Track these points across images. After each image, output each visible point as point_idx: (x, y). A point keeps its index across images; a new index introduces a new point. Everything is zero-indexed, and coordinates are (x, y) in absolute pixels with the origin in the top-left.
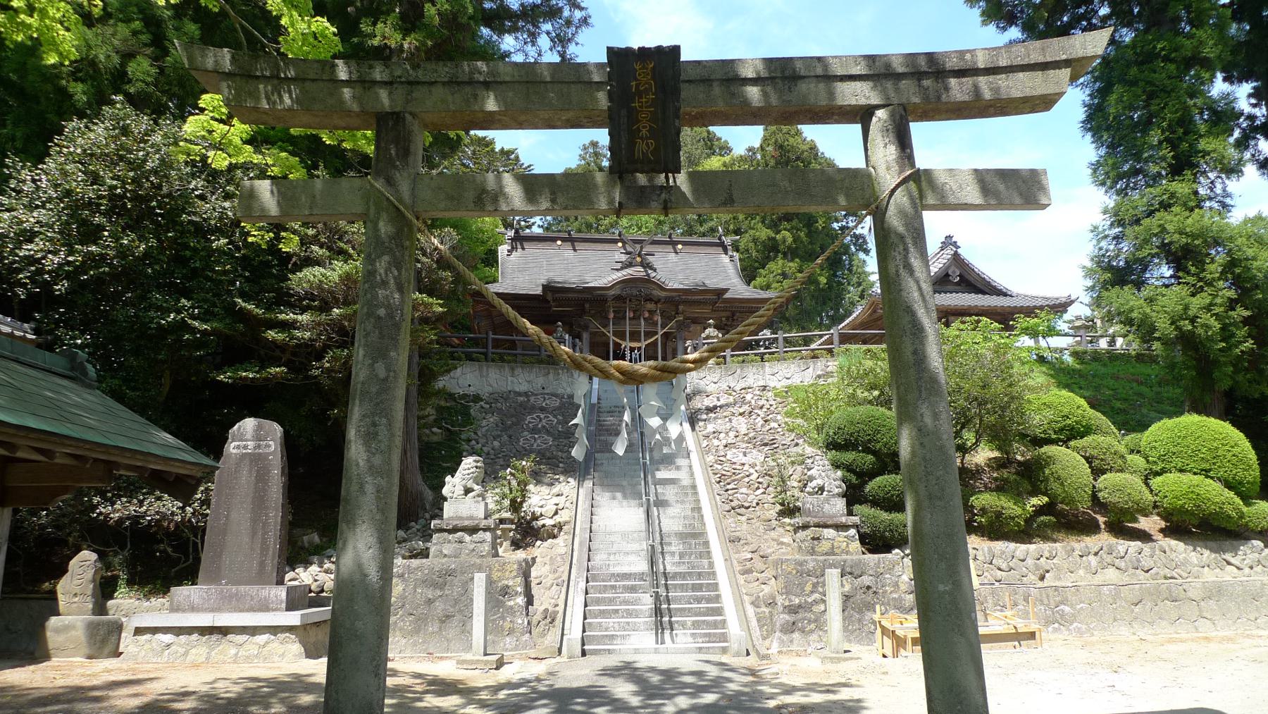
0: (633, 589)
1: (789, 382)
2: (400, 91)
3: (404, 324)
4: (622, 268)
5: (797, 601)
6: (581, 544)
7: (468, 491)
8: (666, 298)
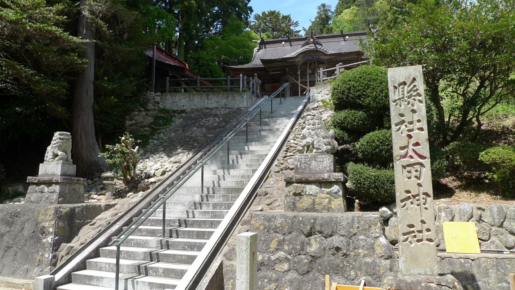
8: (328, 60)
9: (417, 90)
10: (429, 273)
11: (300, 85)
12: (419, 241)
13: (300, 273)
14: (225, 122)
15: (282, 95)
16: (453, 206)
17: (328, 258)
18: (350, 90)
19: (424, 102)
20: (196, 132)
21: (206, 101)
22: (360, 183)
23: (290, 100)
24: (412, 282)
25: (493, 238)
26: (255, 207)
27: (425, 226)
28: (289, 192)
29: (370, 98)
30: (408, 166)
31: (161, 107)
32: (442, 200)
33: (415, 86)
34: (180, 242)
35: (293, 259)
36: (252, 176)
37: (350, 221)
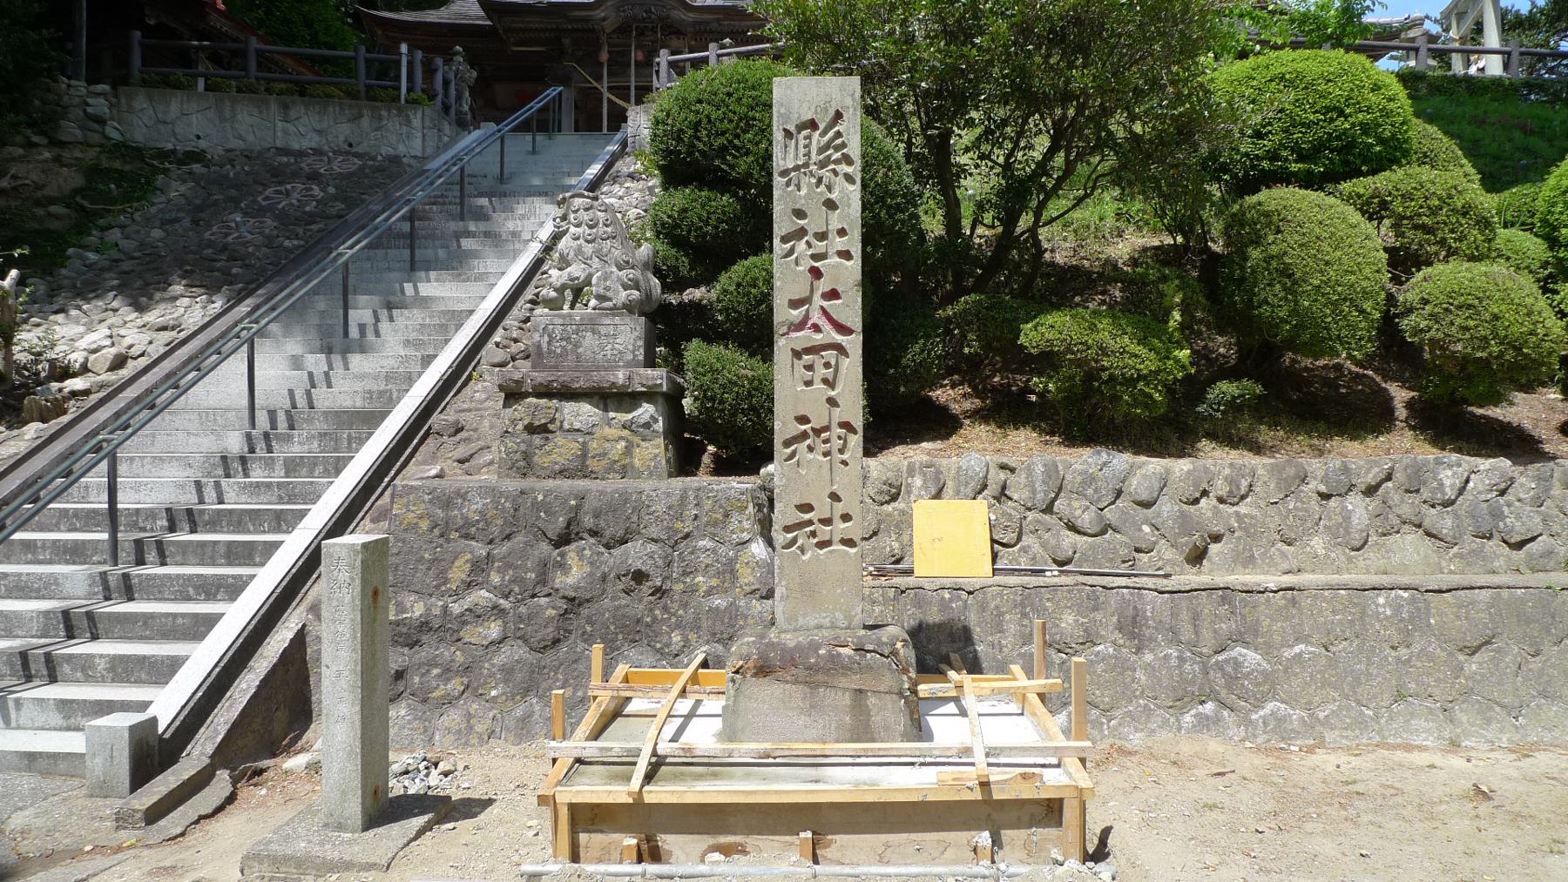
5: (418, 610)
8: (695, 23)
9: (844, 145)
10: (842, 623)
11: (606, 95)
12: (822, 545)
13: (535, 645)
14: (345, 200)
15: (544, 124)
16: (944, 462)
17: (612, 602)
18: (697, 130)
19: (859, 181)
20: (241, 227)
21: (280, 124)
22: (712, 399)
23: (567, 142)
24: (798, 647)
25: (1027, 540)
26: (419, 472)
27: (840, 508)
28: (514, 422)
29: (751, 158)
30: (808, 351)
31: (115, 135)
32: (924, 444)
33: (839, 134)
34: (168, 576)
35: (515, 608)
36: (420, 374)
37: (674, 500)
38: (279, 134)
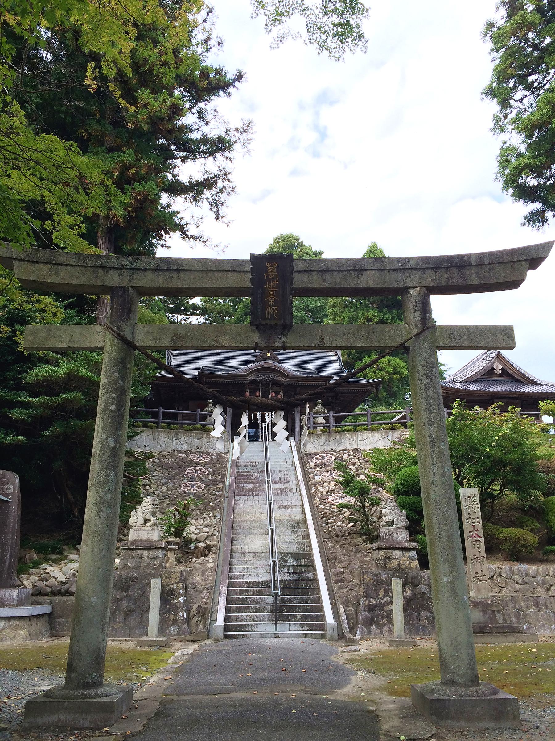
0: (260, 593)
1: (375, 446)
2: (126, 273)
3: (125, 414)
4: (255, 361)
5: (374, 602)
6: (224, 560)
7: (146, 521)
12: (481, 581)
21: (174, 441)
38: (174, 444)
